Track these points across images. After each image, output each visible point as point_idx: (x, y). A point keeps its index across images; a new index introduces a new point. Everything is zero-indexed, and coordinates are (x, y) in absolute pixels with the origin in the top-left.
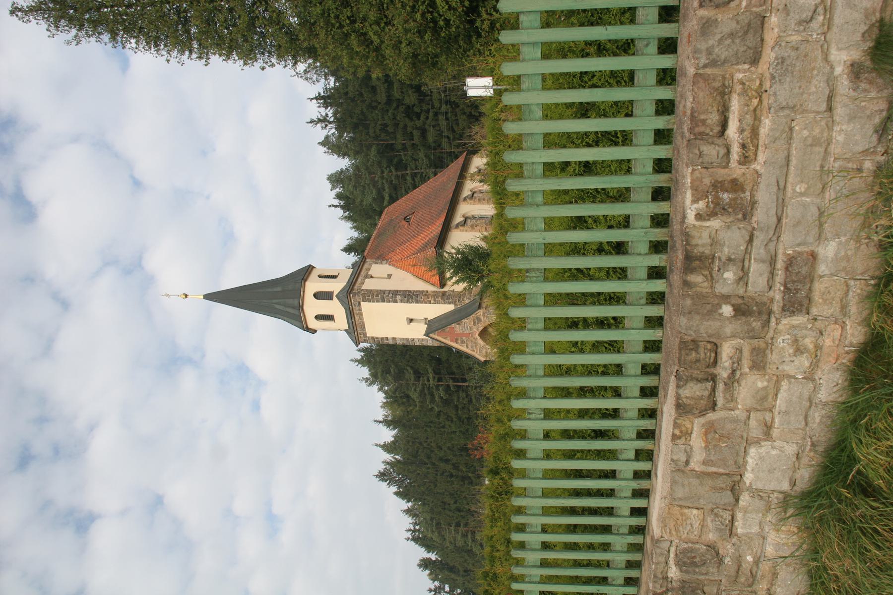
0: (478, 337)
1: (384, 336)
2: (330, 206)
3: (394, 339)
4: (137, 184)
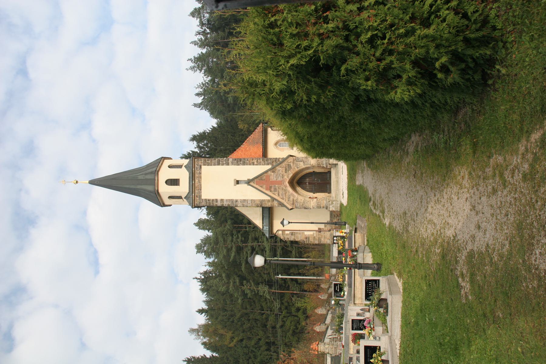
0: (288, 185)
1: (214, 198)
2: (194, 278)
3: (222, 200)
4: (83, 346)
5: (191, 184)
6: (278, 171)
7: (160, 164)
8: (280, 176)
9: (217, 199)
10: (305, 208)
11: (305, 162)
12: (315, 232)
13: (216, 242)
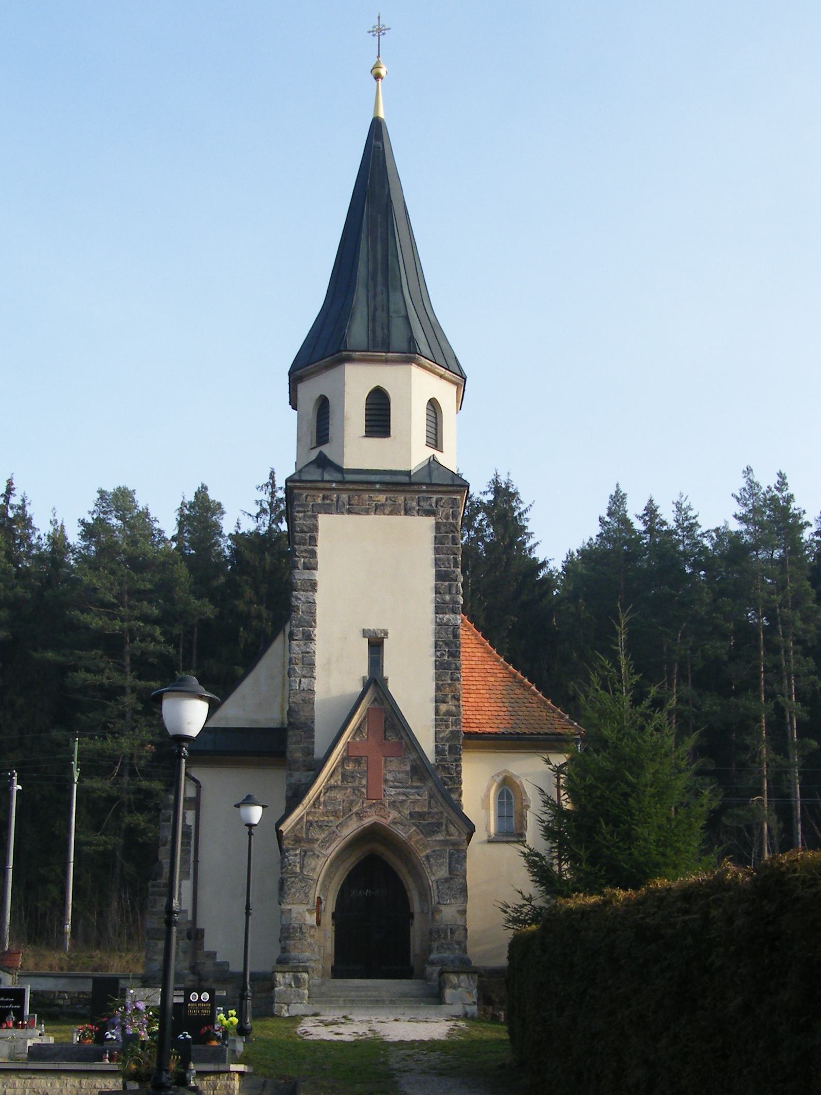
0: (367, 821)
5: (373, 478)
6: (417, 787)
7: (442, 371)
8: (399, 794)
9: (315, 569)
10: (282, 883)
11: (447, 885)
12: (190, 918)
13: (138, 564)
